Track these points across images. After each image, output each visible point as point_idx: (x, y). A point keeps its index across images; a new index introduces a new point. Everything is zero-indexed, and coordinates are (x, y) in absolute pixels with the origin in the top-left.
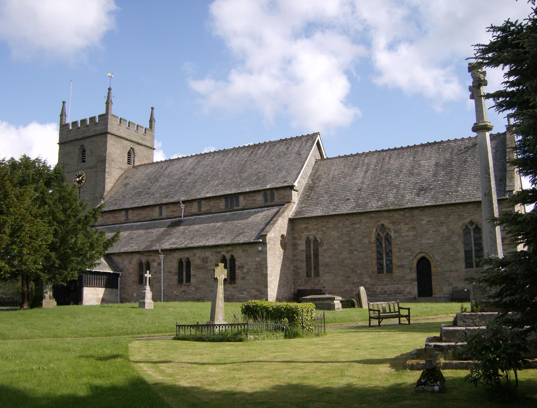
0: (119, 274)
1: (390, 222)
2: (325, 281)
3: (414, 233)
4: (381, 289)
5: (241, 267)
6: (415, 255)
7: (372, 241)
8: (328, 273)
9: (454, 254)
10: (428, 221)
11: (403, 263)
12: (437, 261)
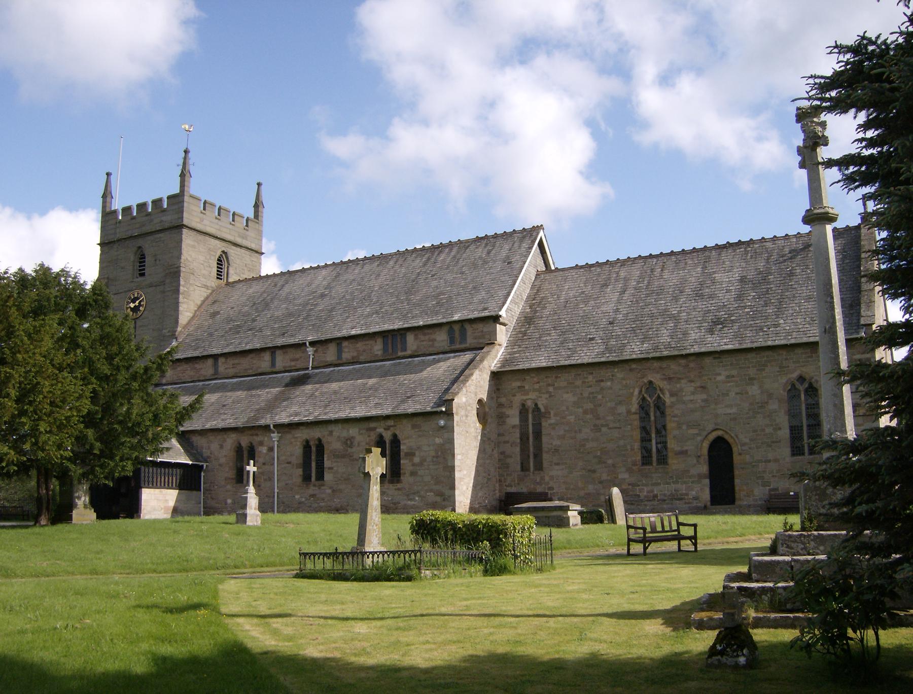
0: (203, 466)
1: (663, 377)
2: (552, 478)
3: (704, 396)
4: (648, 492)
5: (410, 455)
6: (705, 433)
7: (633, 410)
8: (558, 464)
9: (772, 432)
10: (728, 377)
11: (685, 448)
12: (743, 445)
